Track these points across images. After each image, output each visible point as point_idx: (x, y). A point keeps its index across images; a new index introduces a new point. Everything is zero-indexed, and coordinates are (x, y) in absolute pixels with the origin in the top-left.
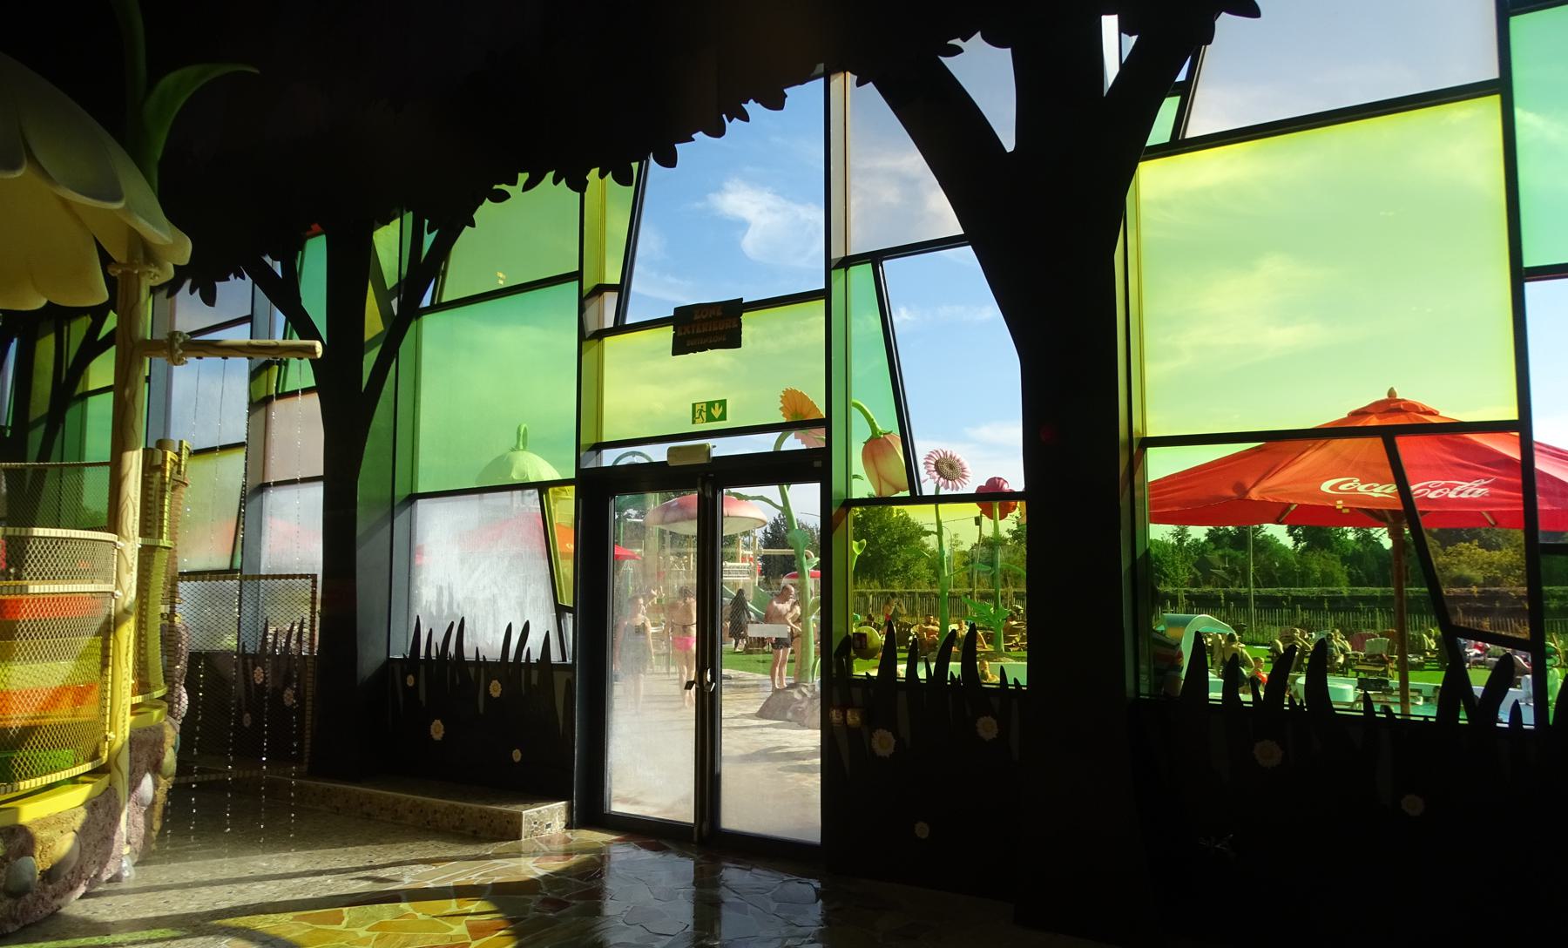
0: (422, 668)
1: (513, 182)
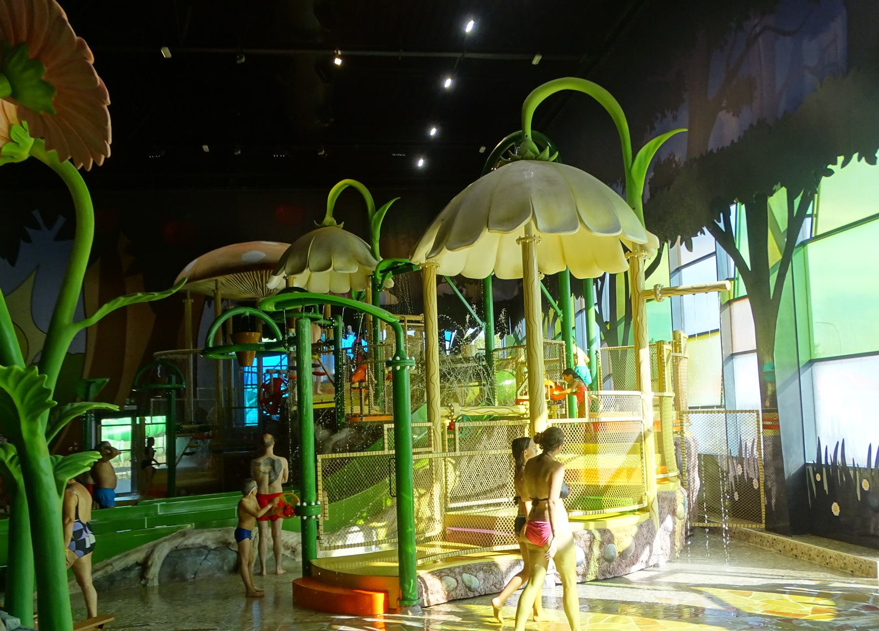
0: (824, 470)
1: (835, 163)
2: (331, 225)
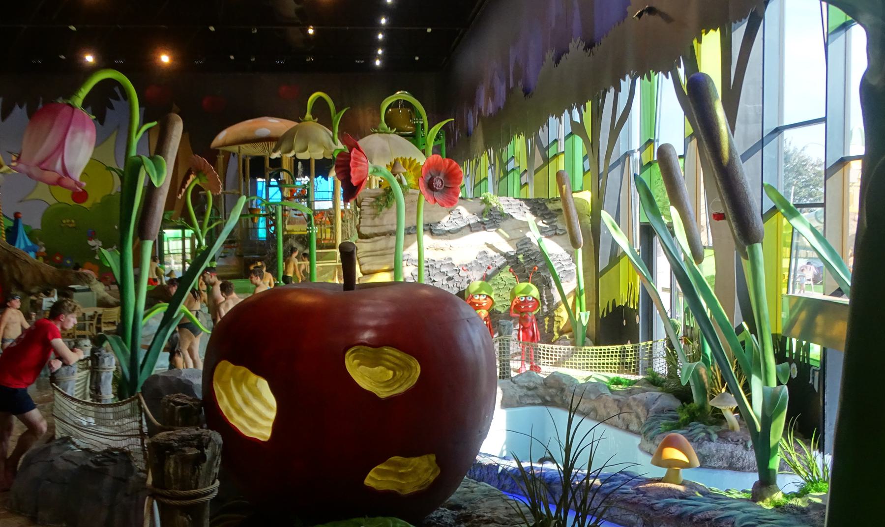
2: (310, 120)
